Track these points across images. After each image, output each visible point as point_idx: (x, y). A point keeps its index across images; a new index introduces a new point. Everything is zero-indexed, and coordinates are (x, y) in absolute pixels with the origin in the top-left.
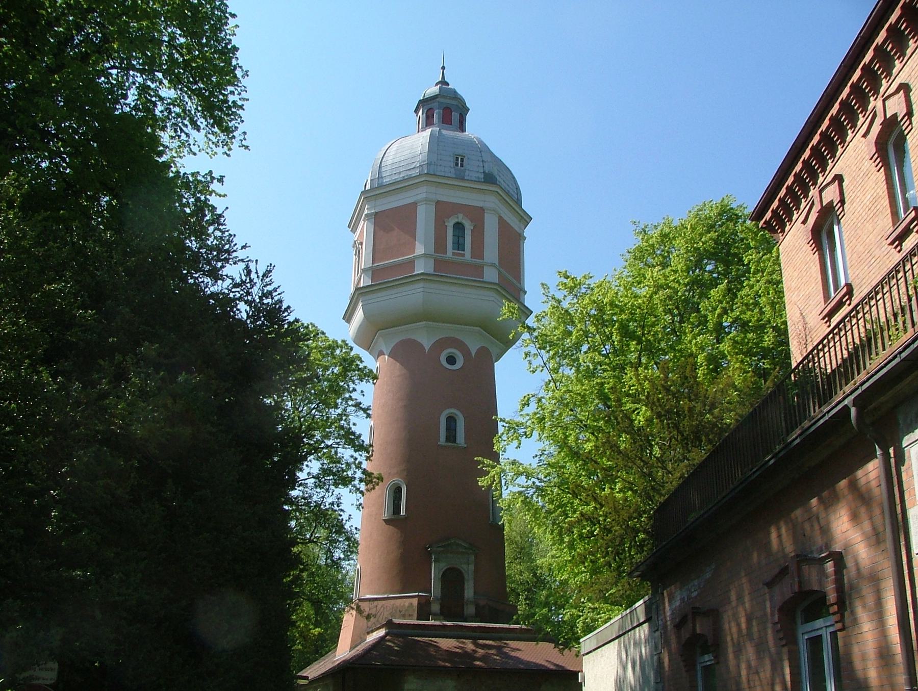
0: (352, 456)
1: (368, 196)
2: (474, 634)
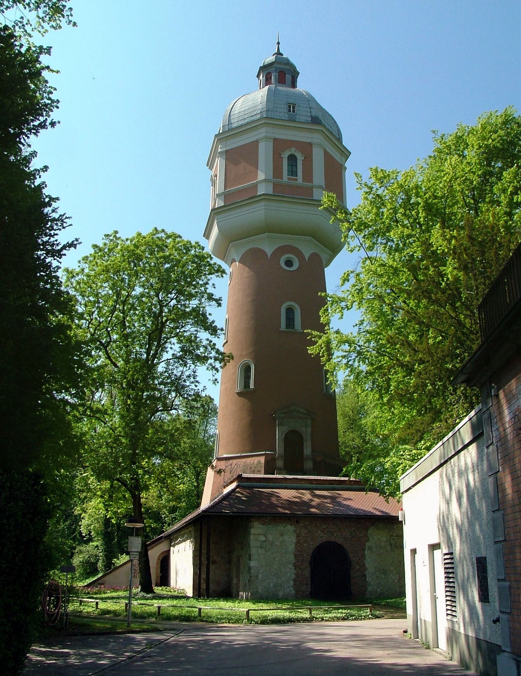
0: (207, 340)
1: (220, 138)
2: (309, 486)
